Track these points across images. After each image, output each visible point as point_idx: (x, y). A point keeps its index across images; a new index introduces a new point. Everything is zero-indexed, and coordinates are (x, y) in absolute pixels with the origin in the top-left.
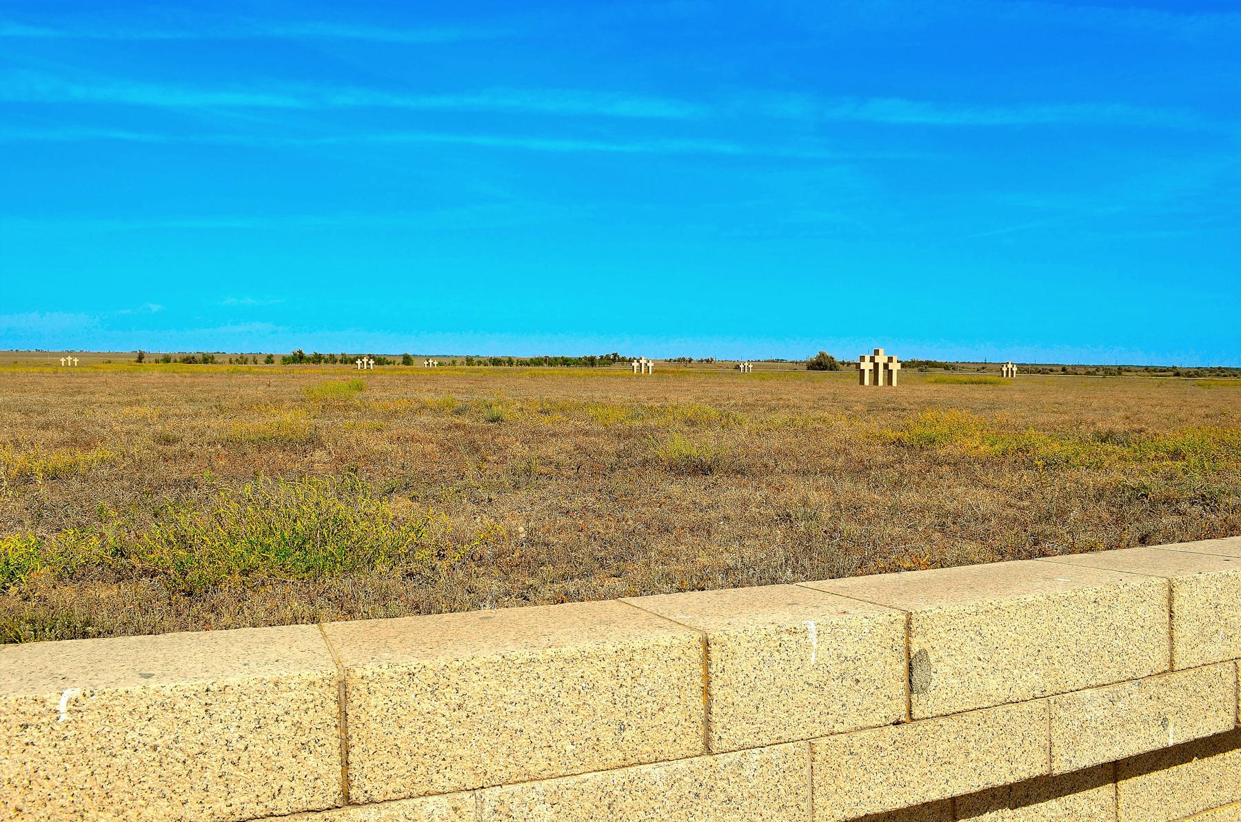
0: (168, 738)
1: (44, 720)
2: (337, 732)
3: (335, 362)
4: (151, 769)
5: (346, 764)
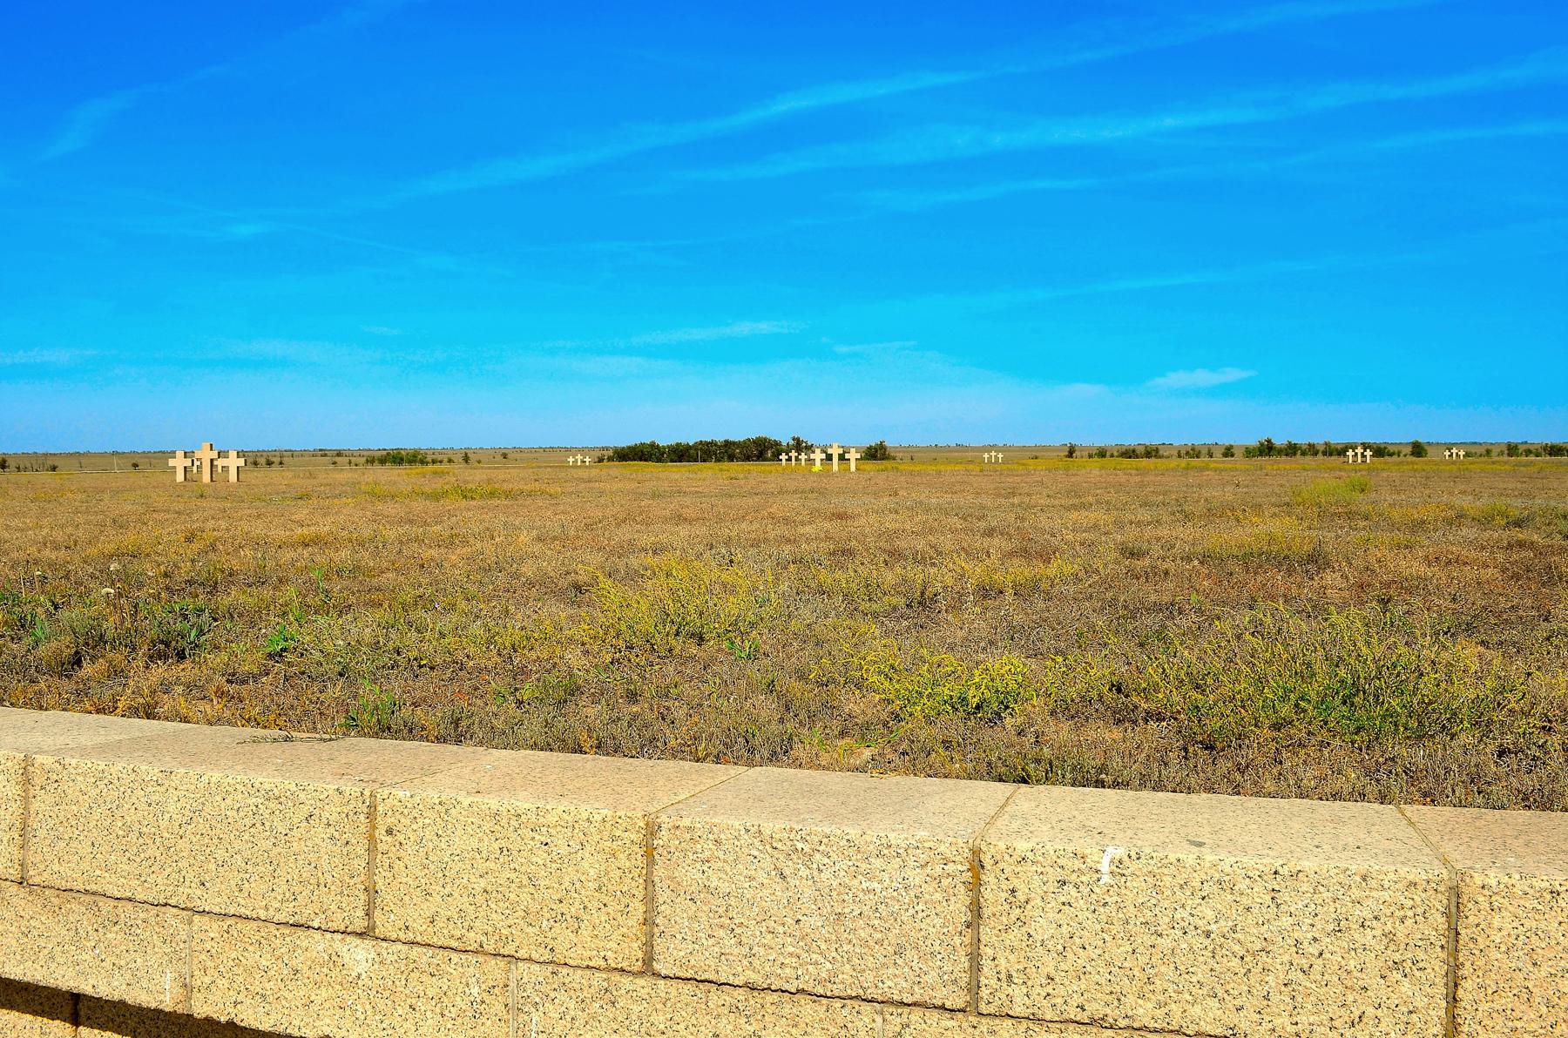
0: (1225, 925)
1: (1084, 879)
2: (1443, 955)
3: (1316, 454)
4: (1201, 959)
5: (1453, 1000)
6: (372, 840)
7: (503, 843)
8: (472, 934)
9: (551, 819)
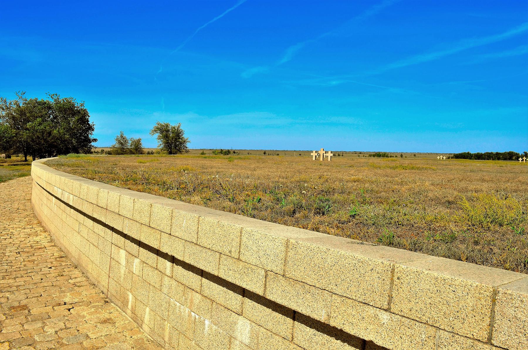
6: (392, 280)
7: (438, 288)
8: (424, 317)
9: (457, 283)
